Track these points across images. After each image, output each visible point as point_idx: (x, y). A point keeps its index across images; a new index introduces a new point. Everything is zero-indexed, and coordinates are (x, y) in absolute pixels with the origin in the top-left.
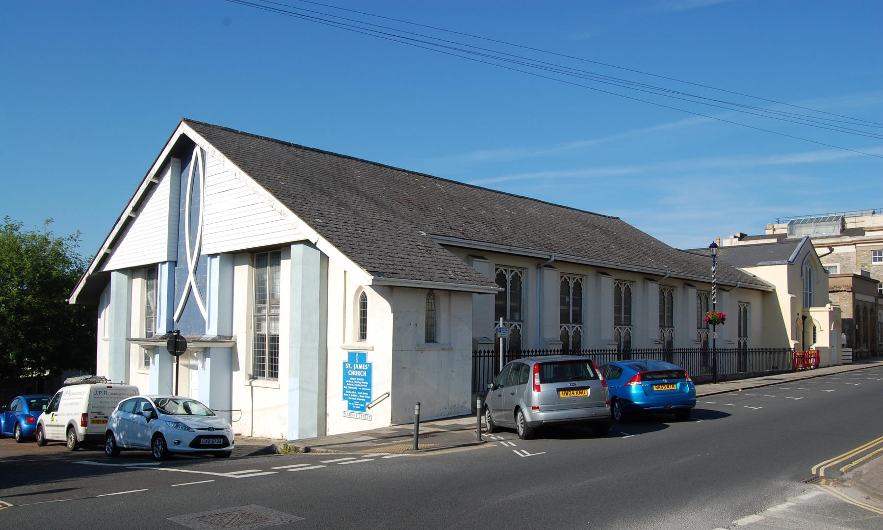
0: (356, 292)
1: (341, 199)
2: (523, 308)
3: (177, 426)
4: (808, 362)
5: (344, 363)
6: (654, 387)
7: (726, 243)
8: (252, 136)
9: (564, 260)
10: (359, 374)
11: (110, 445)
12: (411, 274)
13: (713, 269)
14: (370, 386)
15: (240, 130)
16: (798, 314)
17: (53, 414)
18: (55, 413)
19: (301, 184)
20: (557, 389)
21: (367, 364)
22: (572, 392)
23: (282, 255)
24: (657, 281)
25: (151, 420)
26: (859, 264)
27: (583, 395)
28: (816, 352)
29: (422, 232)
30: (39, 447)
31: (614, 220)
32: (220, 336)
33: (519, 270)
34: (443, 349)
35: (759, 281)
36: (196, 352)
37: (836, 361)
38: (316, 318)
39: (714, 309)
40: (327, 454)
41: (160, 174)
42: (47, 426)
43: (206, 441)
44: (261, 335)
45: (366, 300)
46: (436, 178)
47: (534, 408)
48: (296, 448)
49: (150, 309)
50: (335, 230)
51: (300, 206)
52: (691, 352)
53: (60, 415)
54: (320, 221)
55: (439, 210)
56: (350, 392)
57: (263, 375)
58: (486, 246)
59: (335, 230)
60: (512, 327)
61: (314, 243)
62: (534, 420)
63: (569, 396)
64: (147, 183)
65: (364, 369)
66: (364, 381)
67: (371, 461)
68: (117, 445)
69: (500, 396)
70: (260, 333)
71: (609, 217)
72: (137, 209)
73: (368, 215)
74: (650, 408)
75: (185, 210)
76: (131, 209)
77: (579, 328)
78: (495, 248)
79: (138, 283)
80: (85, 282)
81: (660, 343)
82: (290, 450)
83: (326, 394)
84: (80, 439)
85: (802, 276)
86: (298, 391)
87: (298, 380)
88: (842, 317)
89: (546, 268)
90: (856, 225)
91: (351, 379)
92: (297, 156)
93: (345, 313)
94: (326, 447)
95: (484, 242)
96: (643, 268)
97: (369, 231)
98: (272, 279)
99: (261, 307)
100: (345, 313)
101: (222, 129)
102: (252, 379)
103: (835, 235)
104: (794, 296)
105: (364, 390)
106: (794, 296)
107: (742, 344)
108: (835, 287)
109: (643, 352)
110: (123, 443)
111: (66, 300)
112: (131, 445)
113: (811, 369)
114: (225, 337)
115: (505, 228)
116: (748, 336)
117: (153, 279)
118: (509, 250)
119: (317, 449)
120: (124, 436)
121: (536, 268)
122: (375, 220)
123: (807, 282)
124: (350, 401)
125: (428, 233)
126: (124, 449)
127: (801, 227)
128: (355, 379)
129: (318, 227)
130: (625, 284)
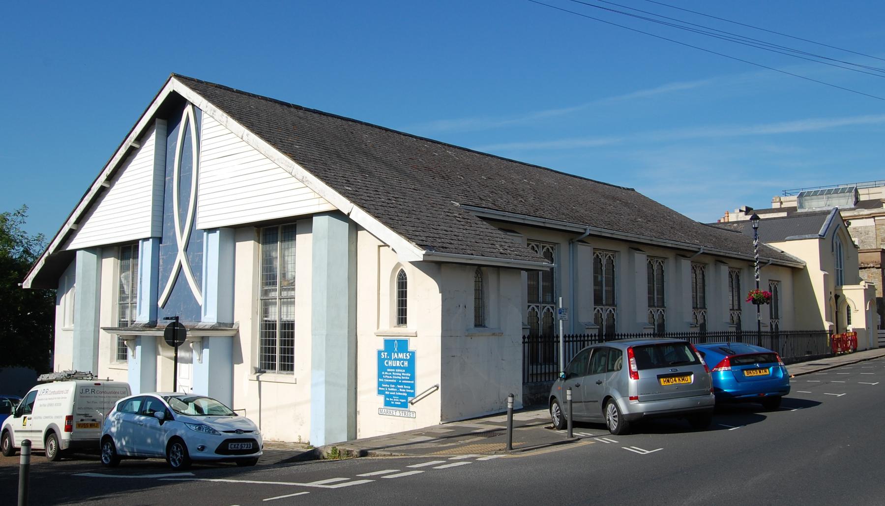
0: (393, 269)
1: (362, 166)
2: (556, 288)
3: (200, 429)
4: (846, 345)
5: (379, 352)
6: (745, 372)
7: (733, 218)
8: (249, 95)
9: (599, 234)
10: (398, 365)
11: (107, 453)
12: (461, 248)
13: (755, 243)
14: (413, 378)
15: (235, 88)
16: (831, 292)
17: (25, 418)
18: (28, 416)
19: (316, 148)
20: (658, 376)
21: (409, 352)
22: (674, 379)
23: (298, 230)
24: (689, 257)
25: (165, 422)
26: (879, 239)
27: (686, 382)
28: (853, 334)
29: (456, 203)
30: (5, 457)
31: (630, 192)
32: (219, 323)
33: (551, 246)
34: (494, 334)
35: (788, 257)
36: (192, 342)
37: (872, 344)
38: (344, 301)
39: (758, 287)
40: (391, 457)
41: (142, 138)
42: (16, 431)
43: (235, 445)
44: (269, 321)
45: (406, 279)
46: (445, 144)
47: (631, 398)
48: (348, 451)
49: (125, 293)
50: (368, 198)
51: (324, 172)
52: (577, 341)
53: (35, 418)
54: (350, 189)
55: (461, 179)
56: (386, 386)
57: (273, 367)
58: (607, 233)
59: (368, 198)
60: (545, 310)
61: (346, 213)
62: (632, 412)
63: (671, 383)
64: (126, 146)
65: (405, 358)
66: (404, 373)
67: (469, 464)
68: (118, 453)
69: (578, 386)
70: (269, 319)
71: (624, 188)
72: (112, 178)
73: (395, 182)
74: (742, 396)
75: (173, 178)
76: (106, 178)
77: (550, 309)
78: (530, 220)
79: (110, 264)
80: (44, 262)
81: (696, 326)
82: (339, 454)
83: (356, 388)
84: (64, 447)
85: (833, 251)
86: (324, 385)
87: (323, 372)
88: (876, 297)
89: (580, 243)
90: (869, 197)
91: (389, 370)
92: (300, 118)
93: (379, 294)
94: (385, 449)
95: (518, 213)
96: (677, 243)
97: (402, 200)
98: (283, 256)
99: (270, 290)
100: (379, 294)
101: (216, 87)
102: (259, 372)
103: (848, 207)
104: (827, 273)
105: (405, 383)
106: (827, 273)
107: (774, 327)
108: (862, 263)
109: (582, 338)
110: (126, 449)
111: (19, 284)
112: (137, 453)
113: (850, 353)
114: (225, 325)
115: (531, 199)
116: (779, 317)
117: (129, 259)
118: (544, 223)
119: (377, 452)
120: (127, 443)
121: (568, 244)
122: (403, 189)
123: (837, 259)
124: (386, 396)
125: (461, 203)
126: (126, 457)
127: (812, 199)
128: (394, 370)
129: (350, 196)
130: (657, 261)
